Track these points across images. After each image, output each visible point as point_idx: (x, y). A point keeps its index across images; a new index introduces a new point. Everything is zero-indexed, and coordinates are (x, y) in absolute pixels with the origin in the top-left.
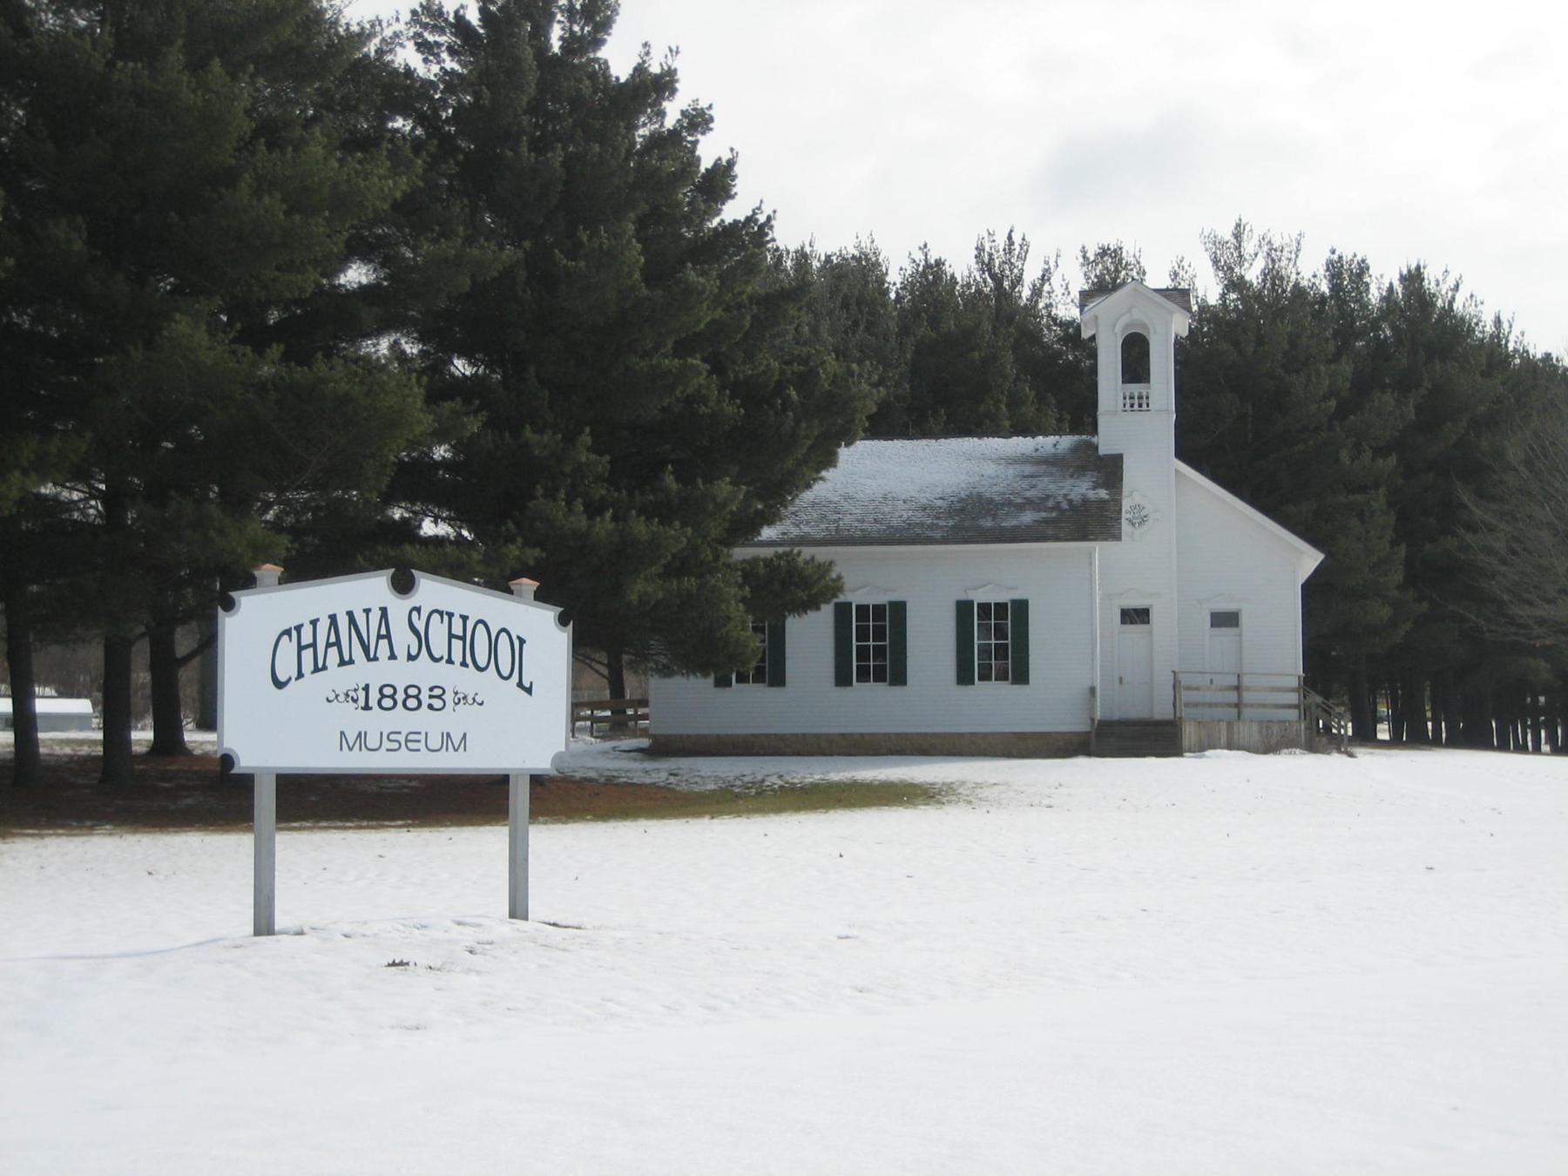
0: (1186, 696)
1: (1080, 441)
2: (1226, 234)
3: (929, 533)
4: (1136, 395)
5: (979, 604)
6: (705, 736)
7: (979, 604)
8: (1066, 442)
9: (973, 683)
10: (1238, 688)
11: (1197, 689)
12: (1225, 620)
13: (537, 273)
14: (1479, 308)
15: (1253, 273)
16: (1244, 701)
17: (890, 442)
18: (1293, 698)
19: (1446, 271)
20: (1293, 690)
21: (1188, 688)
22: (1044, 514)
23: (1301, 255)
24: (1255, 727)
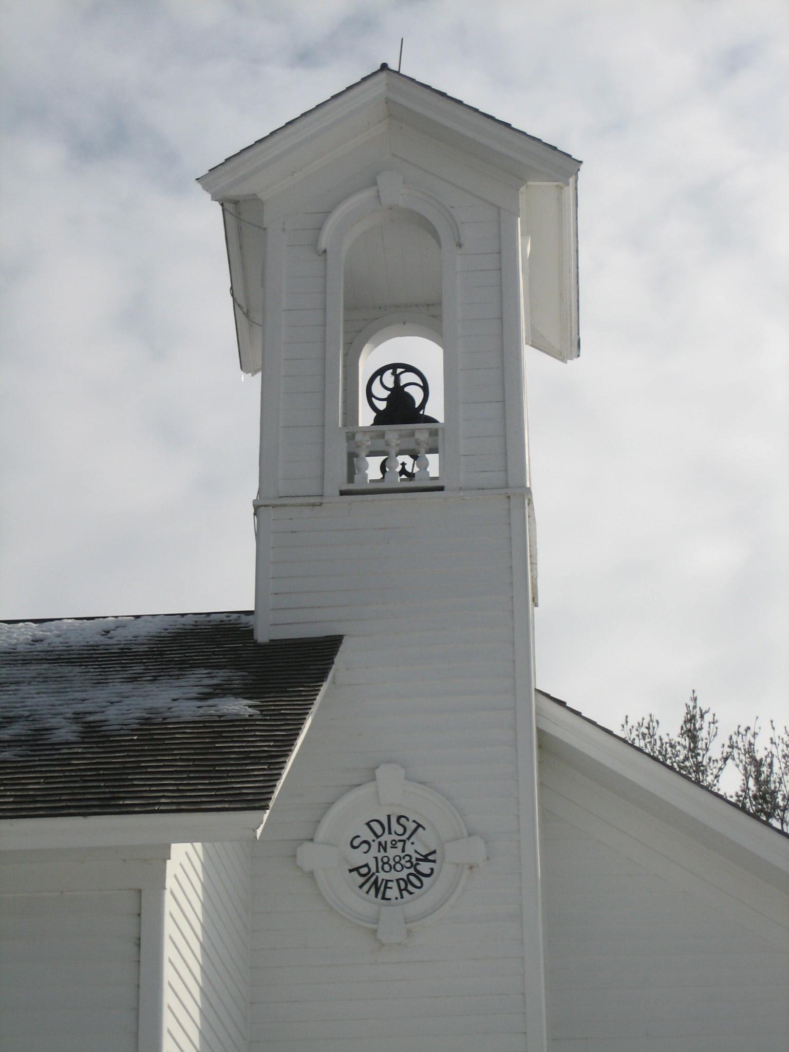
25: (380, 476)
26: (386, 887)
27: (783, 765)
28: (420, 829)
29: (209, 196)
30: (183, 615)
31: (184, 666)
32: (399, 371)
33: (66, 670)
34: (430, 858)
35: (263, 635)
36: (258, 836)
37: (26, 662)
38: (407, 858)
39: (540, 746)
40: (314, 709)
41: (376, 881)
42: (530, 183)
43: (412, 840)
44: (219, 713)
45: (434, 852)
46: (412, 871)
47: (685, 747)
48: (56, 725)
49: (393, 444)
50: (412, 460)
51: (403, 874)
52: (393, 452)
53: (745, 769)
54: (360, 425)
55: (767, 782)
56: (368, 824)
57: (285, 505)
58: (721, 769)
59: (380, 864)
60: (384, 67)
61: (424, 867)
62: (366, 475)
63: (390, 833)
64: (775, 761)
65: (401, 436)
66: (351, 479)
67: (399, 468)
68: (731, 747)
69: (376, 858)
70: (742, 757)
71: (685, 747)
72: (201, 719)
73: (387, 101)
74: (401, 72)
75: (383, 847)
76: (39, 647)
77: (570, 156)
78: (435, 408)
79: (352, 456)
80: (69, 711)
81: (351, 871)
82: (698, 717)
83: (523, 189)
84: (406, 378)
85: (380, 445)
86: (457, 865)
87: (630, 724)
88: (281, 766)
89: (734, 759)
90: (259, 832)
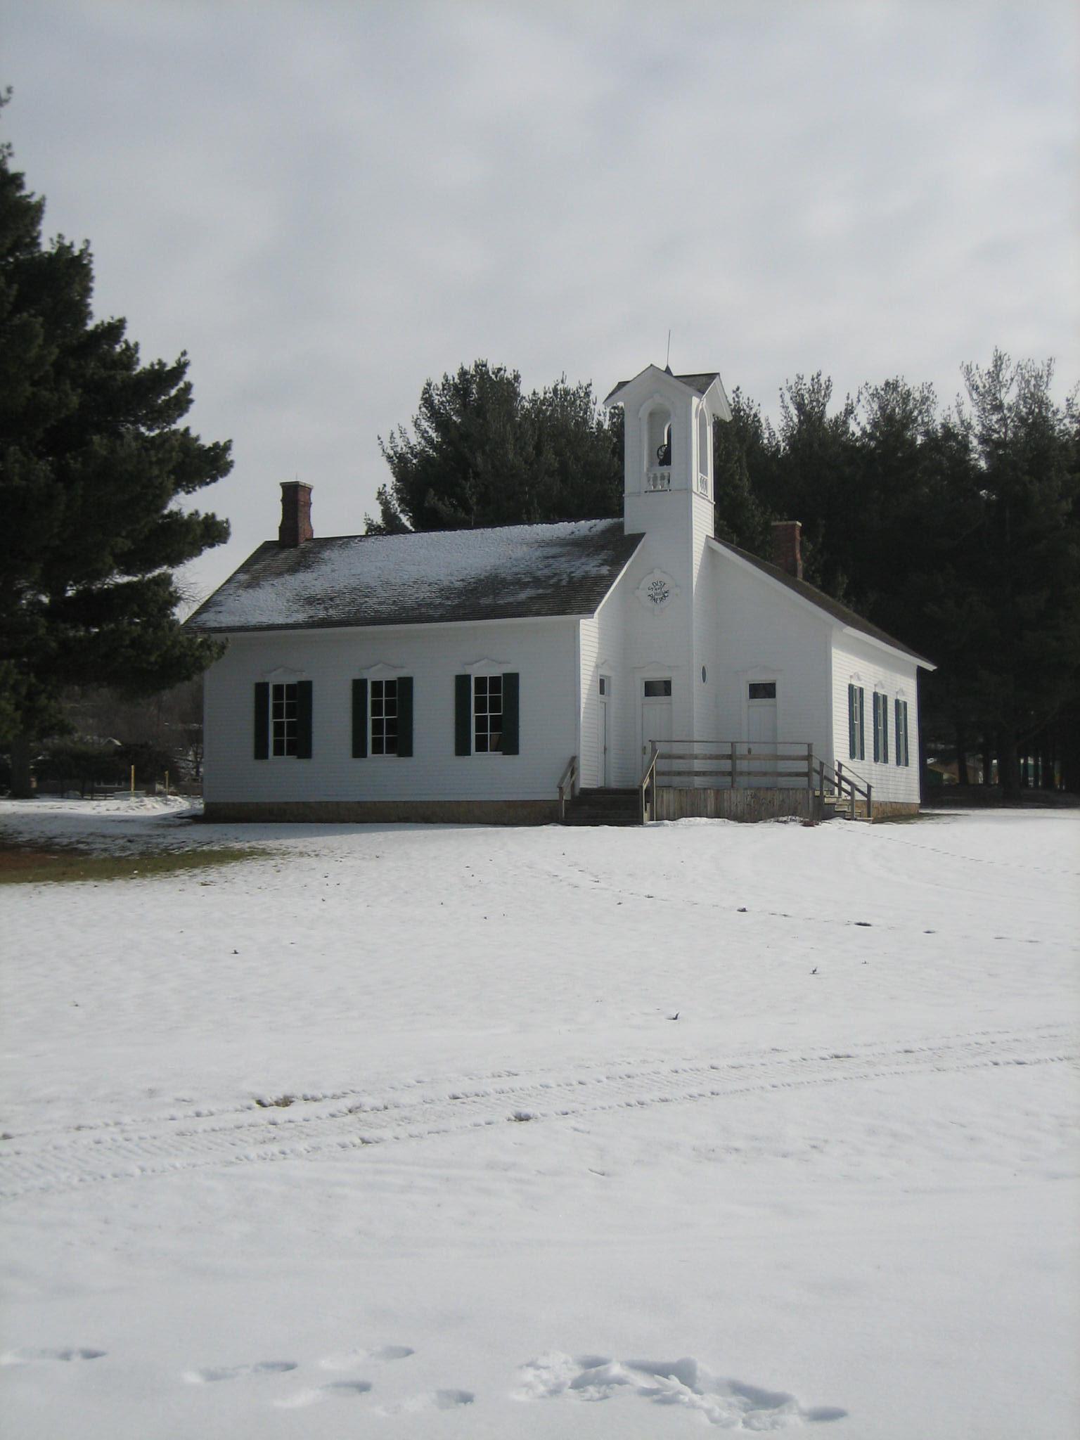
1: (615, 523)
2: (987, 365)
3: (431, 612)
4: (659, 475)
5: (476, 678)
6: (247, 804)
7: (476, 678)
8: (600, 524)
9: (469, 754)
12: (763, 691)
13: (983, 492)
15: (1009, 397)
16: (738, 770)
17: (453, 532)
22: (540, 591)
61: (666, 595)
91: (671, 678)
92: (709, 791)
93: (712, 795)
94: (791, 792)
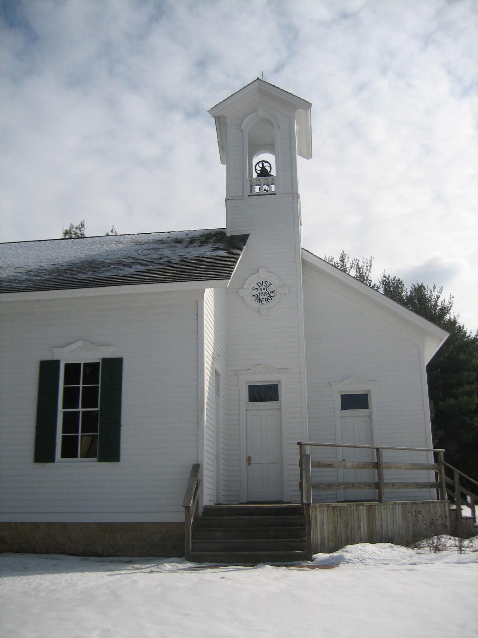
0: (315, 474)
10: (377, 465)
11: (330, 466)
14: (451, 300)
18: (430, 476)
19: (435, 287)
20: (427, 467)
21: (319, 465)
23: (372, 267)
24: (399, 511)
25: (259, 191)
26: (262, 300)
27: (366, 269)
28: (271, 285)
29: (211, 116)
30: (207, 230)
31: (208, 243)
32: (263, 162)
33: (176, 244)
34: (274, 292)
35: (228, 234)
36: (228, 286)
37: (166, 243)
38: (268, 292)
39: (302, 263)
40: (242, 253)
41: (260, 298)
42: (298, 110)
43: (269, 288)
44: (217, 255)
45: (275, 291)
46: (269, 296)
47: (341, 264)
48: (174, 259)
49: (262, 182)
50: (267, 187)
51: (267, 297)
52: (262, 185)
53: (356, 270)
54: (253, 177)
55: (362, 273)
56: (257, 284)
57: (233, 199)
58: (350, 270)
59: (260, 294)
60: (258, 78)
61: (272, 295)
62: (255, 191)
63: (263, 286)
64: (364, 268)
65: (264, 180)
66: (251, 192)
67: (264, 189)
68: (352, 264)
69: (259, 293)
70: (355, 267)
71: (341, 264)
72: (212, 256)
73: (259, 88)
74: (263, 80)
75: (261, 290)
76: (169, 239)
77: (309, 102)
78: (273, 173)
79: (251, 186)
80: (177, 255)
81: (253, 296)
82: (344, 256)
83: (296, 112)
84: (265, 164)
85: (259, 183)
86: (281, 294)
87: (326, 258)
88: (233, 268)
89: (353, 267)
90: (228, 285)
91: (280, 381)
92: (361, 507)
93: (365, 512)
94: (431, 505)
